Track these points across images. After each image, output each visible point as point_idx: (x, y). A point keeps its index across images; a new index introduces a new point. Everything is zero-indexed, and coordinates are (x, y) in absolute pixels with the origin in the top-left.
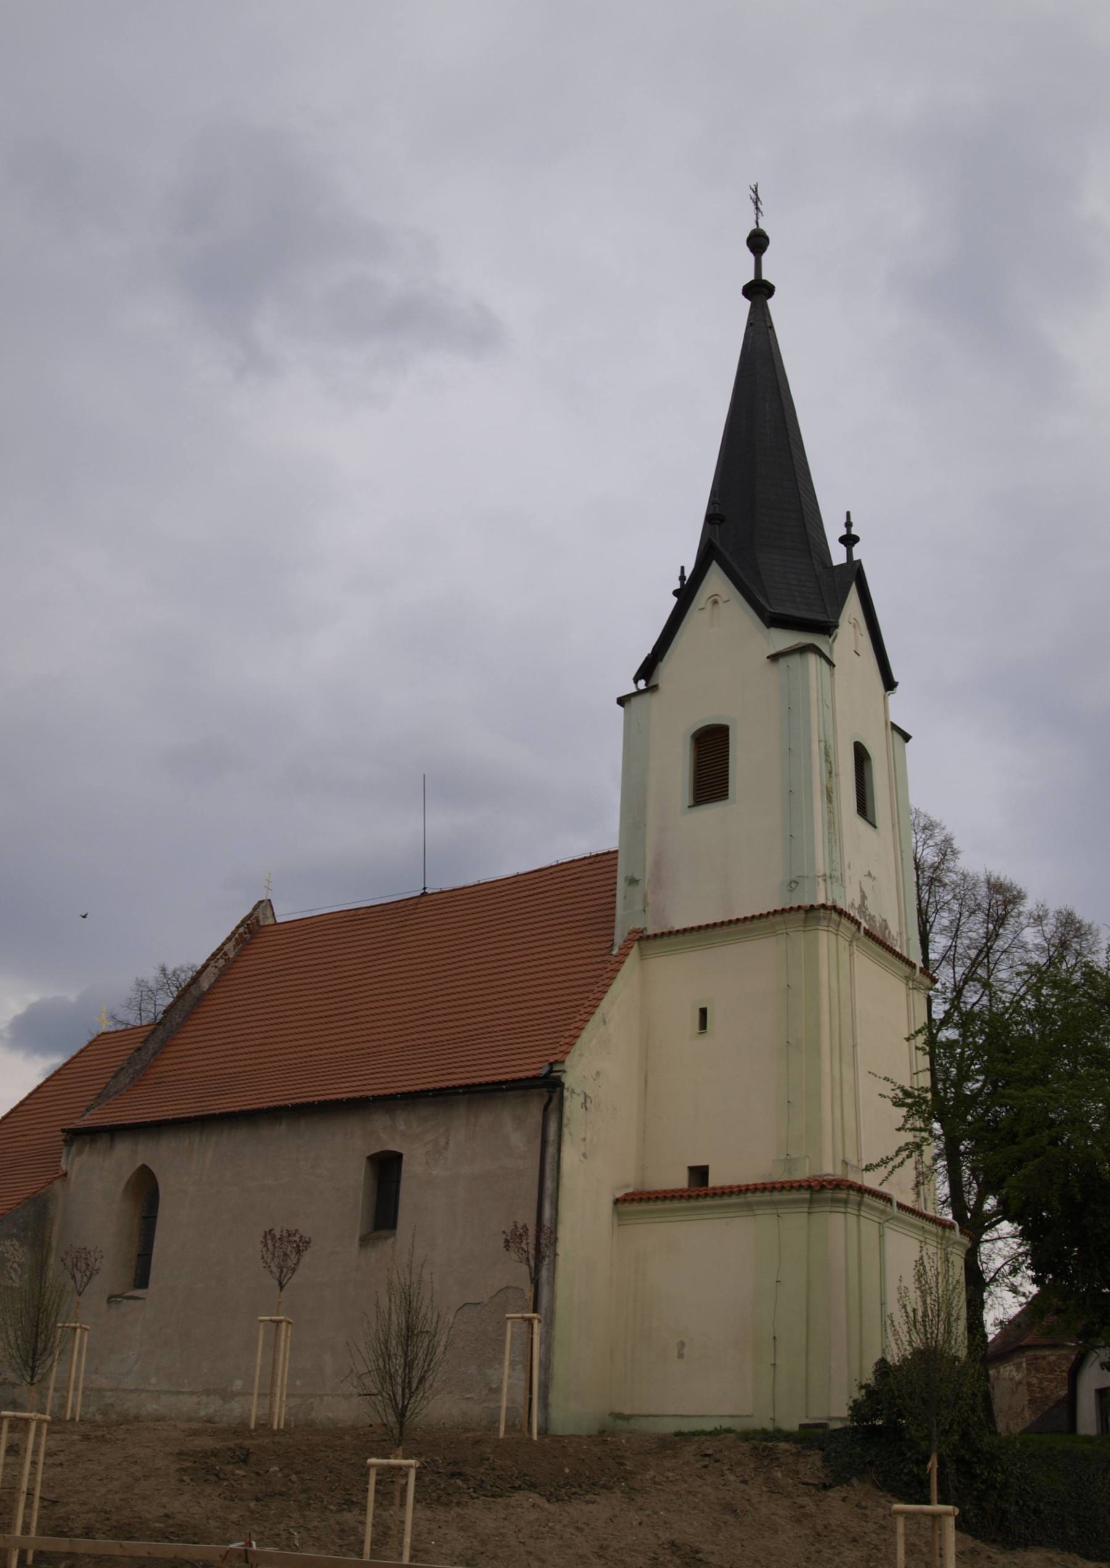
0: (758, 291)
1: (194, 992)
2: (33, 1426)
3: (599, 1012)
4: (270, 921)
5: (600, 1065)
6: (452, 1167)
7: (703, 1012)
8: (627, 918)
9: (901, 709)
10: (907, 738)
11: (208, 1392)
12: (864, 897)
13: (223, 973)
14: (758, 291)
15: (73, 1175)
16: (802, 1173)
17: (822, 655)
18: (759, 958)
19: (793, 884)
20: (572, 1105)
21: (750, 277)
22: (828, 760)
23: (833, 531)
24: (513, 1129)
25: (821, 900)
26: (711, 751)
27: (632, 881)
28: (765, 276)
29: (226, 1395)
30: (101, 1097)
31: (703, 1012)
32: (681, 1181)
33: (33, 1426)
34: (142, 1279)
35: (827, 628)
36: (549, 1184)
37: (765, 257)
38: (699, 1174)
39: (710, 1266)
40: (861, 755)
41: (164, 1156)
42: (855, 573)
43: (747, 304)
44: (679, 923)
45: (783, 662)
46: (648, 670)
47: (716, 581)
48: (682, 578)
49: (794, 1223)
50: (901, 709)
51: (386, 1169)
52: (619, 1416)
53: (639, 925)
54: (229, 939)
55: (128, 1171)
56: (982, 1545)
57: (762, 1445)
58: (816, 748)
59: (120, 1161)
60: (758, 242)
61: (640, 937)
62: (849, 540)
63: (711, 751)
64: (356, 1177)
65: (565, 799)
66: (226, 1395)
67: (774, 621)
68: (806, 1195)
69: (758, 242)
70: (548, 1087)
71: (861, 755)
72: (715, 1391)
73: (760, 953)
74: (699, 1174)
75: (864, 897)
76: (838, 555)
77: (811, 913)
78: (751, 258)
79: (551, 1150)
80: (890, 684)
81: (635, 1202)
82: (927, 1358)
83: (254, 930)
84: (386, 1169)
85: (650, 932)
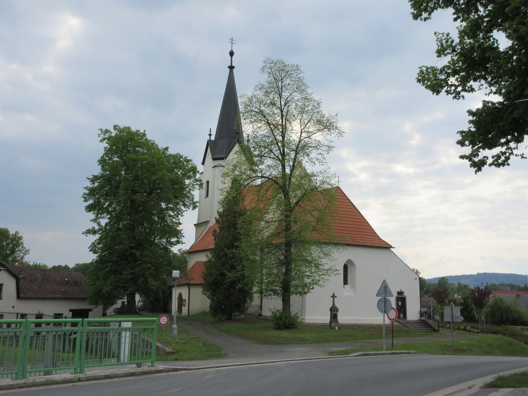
0: (231, 68)
14: (231, 68)
37: (233, 57)
40: (208, 182)
43: (229, 70)
60: (232, 54)
69: (232, 54)
71: (208, 182)
78: (230, 57)
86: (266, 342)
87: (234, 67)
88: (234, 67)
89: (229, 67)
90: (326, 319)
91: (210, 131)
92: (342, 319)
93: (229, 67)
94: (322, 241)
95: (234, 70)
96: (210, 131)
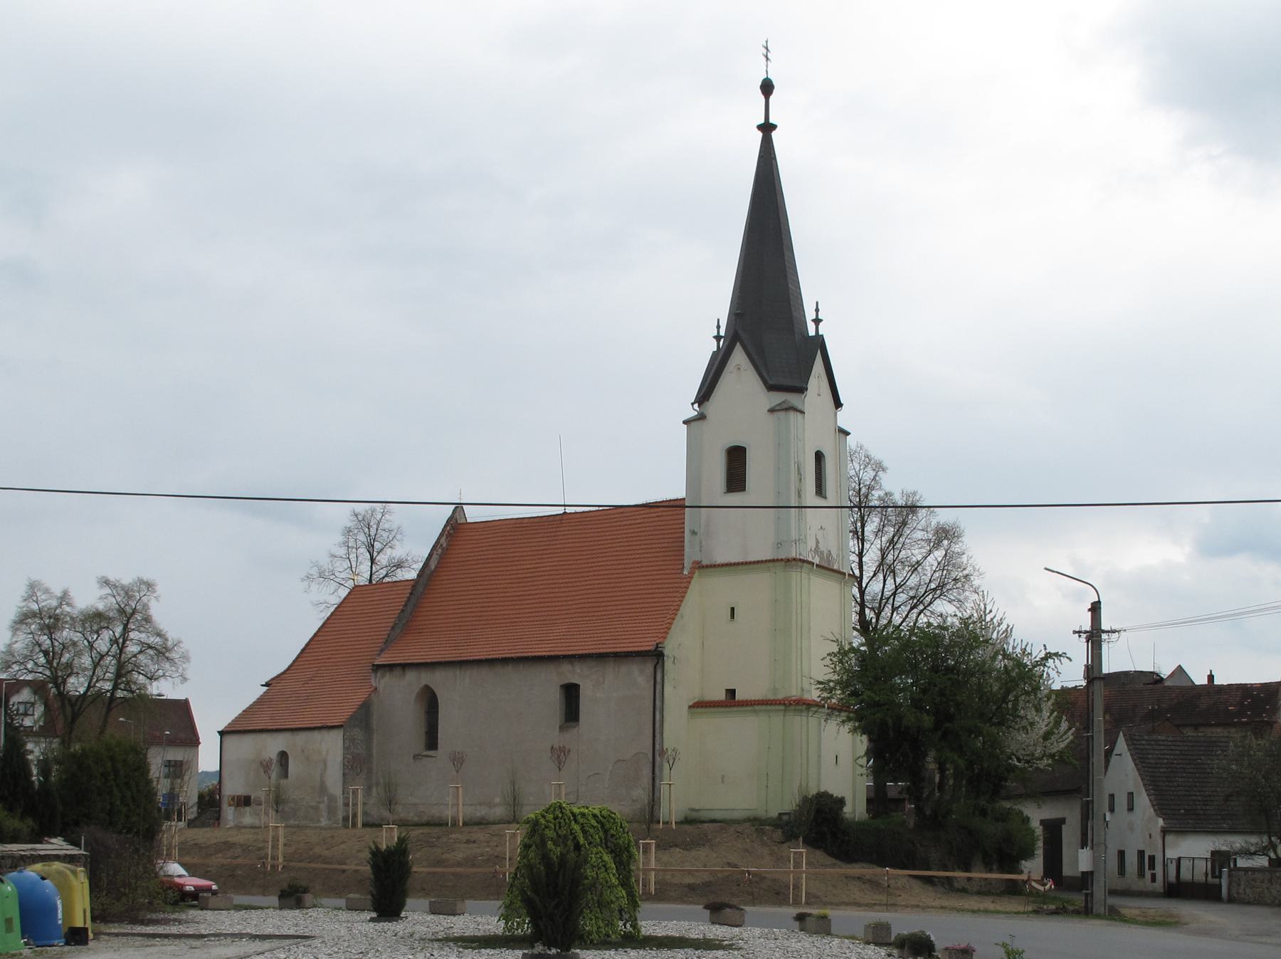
0: (767, 128)
1: (428, 572)
2: (360, 825)
3: (679, 613)
4: (463, 521)
5: (683, 643)
6: (604, 692)
7: (733, 609)
9: (843, 419)
10: (848, 434)
11: (480, 804)
12: (818, 542)
13: (442, 557)
14: (767, 128)
15: (381, 689)
16: (780, 696)
17: (796, 410)
18: (761, 582)
19: (779, 545)
20: (668, 664)
21: (762, 121)
22: (799, 473)
23: (810, 315)
24: (639, 675)
25: (793, 555)
26: (736, 457)
27: (694, 533)
28: (771, 121)
29: (490, 805)
30: (388, 643)
31: (733, 609)
32: (722, 696)
33: (360, 825)
35: (801, 390)
36: (658, 703)
37: (772, 98)
38: (731, 693)
39: (738, 737)
40: (819, 456)
43: (760, 134)
45: (776, 414)
50: (843, 419)
51: (571, 693)
52: (693, 810)
53: (698, 559)
54: (441, 535)
55: (417, 688)
56: (879, 870)
57: (757, 823)
58: (793, 468)
59: (413, 681)
60: (767, 88)
61: (699, 566)
62: (817, 321)
63: (736, 457)
64: (555, 697)
66: (490, 805)
67: (771, 388)
68: (782, 707)
69: (767, 88)
70: (657, 656)
71: (819, 456)
72: (740, 797)
74: (731, 693)
75: (818, 542)
76: (812, 332)
78: (762, 98)
79: (659, 687)
80: (838, 404)
81: (701, 706)
83: (456, 529)
84: (571, 693)
85: (704, 563)
86: (949, 886)
87: (774, 127)
88: (774, 127)
89: (760, 127)
90: (1205, 682)
91: (817, 310)
92: (1216, 682)
93: (760, 127)
94: (476, 828)
95: (774, 134)
96: (817, 310)
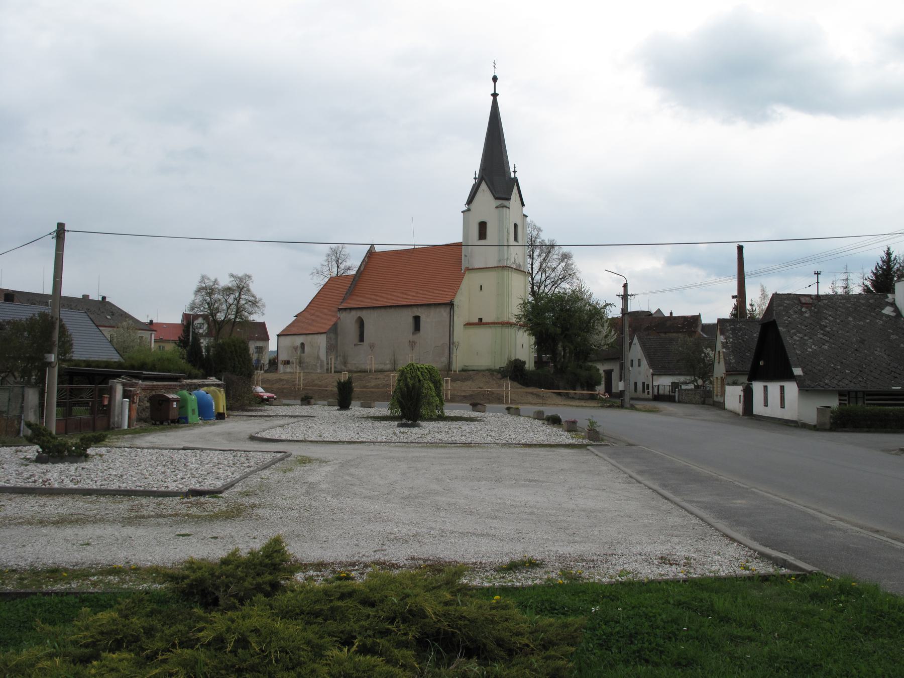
0: (495, 95)
5: (461, 300)
6: (429, 319)
8: (464, 265)
9: (525, 210)
13: (365, 266)
14: (495, 95)
16: (500, 321)
19: (499, 261)
20: (455, 308)
23: (512, 169)
24: (444, 312)
26: (483, 226)
32: (477, 321)
34: (362, 339)
35: (508, 199)
38: (481, 319)
39: (483, 339)
40: (516, 226)
41: (364, 314)
42: (515, 181)
44: (476, 266)
46: (470, 202)
47: (484, 186)
48: (475, 178)
49: (498, 330)
50: (525, 210)
51: (417, 319)
57: (491, 371)
59: (354, 315)
60: (495, 79)
61: (468, 269)
62: (515, 172)
63: (483, 226)
64: (411, 321)
65: (448, 229)
67: (496, 198)
69: (495, 79)
70: (451, 305)
71: (516, 226)
72: (484, 361)
73: (492, 275)
77: (504, 268)
80: (523, 205)
81: (468, 324)
82: (531, 329)
84: (417, 319)
